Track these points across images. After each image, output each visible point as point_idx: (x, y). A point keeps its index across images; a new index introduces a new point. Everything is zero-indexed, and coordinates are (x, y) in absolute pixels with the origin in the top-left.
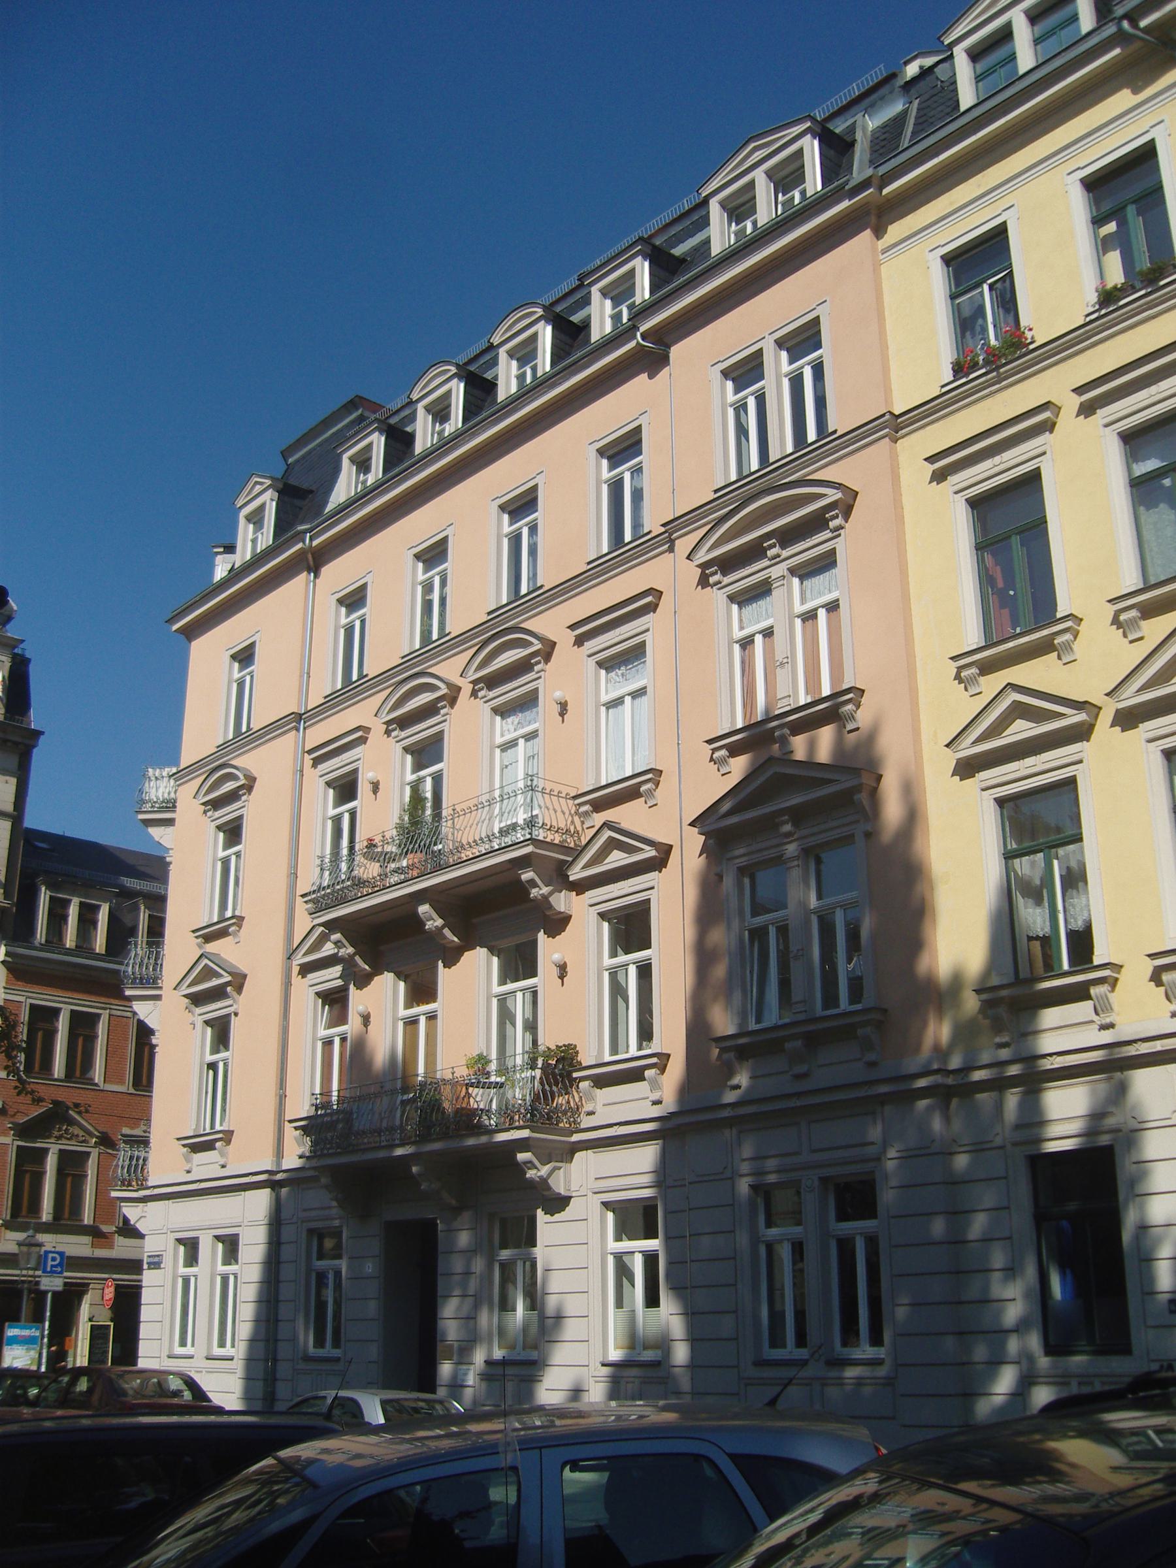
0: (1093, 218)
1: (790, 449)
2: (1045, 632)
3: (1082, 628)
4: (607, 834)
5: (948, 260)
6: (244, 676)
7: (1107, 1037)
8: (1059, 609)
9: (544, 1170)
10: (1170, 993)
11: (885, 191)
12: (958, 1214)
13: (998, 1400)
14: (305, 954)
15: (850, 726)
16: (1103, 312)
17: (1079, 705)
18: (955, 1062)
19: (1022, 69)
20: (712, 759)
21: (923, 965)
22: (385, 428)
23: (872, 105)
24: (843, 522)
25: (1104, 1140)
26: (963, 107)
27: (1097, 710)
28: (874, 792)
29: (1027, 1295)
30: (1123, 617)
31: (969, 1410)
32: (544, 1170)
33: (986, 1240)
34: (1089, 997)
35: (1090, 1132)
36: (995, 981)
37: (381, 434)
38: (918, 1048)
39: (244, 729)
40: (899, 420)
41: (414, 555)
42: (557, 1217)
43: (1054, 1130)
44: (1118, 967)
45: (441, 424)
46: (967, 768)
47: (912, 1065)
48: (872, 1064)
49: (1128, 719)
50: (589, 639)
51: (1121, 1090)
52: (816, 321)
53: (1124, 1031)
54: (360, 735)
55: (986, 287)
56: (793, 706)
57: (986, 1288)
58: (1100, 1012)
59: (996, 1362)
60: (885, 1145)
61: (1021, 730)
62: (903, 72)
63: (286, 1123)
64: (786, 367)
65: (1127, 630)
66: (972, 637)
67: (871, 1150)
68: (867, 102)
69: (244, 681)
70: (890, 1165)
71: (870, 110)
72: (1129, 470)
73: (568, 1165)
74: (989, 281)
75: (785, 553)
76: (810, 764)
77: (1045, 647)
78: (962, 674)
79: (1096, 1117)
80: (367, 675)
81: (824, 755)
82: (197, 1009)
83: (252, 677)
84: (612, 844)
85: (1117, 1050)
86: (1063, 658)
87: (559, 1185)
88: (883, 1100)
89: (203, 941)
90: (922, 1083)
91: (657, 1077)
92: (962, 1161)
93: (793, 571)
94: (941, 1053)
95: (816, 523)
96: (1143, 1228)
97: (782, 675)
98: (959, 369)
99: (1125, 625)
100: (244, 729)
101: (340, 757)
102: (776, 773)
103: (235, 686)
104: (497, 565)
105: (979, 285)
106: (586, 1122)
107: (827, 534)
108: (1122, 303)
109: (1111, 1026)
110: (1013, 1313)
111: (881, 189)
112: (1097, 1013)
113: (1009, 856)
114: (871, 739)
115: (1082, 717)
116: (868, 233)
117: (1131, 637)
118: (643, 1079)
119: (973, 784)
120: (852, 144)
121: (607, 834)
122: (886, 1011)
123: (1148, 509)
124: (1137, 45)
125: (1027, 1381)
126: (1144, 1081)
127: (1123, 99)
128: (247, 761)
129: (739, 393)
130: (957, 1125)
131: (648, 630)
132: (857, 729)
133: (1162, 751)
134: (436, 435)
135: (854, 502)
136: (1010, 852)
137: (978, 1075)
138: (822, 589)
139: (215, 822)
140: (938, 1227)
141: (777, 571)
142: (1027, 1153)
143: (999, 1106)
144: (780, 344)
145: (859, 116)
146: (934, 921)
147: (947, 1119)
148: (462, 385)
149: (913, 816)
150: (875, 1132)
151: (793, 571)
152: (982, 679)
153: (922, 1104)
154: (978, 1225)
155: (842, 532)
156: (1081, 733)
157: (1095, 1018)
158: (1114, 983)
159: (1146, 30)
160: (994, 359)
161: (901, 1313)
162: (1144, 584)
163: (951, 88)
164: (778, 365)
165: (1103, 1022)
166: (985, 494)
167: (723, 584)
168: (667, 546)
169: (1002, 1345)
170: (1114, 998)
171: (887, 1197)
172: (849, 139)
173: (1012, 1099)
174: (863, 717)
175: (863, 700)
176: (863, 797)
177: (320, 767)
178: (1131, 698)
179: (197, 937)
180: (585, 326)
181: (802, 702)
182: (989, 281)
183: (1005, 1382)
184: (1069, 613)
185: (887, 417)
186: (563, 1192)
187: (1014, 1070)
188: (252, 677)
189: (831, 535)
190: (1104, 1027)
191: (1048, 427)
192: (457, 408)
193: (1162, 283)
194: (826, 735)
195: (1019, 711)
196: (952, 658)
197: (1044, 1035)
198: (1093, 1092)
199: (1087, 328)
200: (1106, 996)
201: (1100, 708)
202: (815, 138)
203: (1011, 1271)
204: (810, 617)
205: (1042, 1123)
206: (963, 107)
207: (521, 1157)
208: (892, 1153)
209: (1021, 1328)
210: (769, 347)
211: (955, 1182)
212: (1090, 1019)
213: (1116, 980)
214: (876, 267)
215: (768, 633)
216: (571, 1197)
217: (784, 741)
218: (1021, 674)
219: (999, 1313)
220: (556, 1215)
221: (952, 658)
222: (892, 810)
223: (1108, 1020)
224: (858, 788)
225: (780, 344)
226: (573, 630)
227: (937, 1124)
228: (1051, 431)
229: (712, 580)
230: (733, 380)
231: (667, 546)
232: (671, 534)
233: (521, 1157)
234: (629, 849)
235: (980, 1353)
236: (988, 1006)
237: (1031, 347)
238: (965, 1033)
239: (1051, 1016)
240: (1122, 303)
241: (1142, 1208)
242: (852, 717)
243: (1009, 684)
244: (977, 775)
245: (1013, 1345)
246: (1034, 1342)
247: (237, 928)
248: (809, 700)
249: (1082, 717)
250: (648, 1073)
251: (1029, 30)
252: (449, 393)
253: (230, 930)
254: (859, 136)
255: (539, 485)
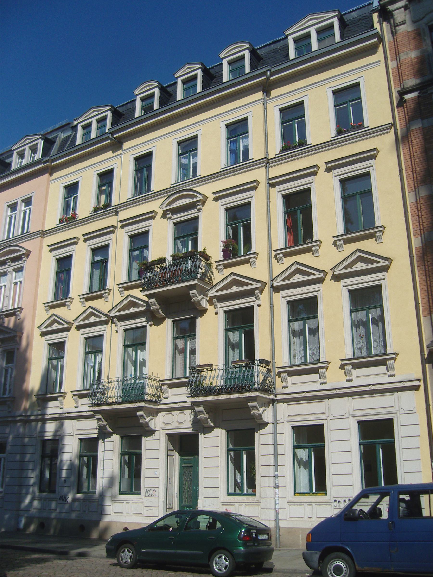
0: (281, 122)
1: (20, 234)
2: (64, 301)
3: (322, 245)
4: (91, 310)
5: (65, 187)
6: (27, 210)
7: (61, 411)
8: (314, 237)
9: (148, 419)
10: (346, 373)
11: (53, 164)
12: (23, 454)
13: (26, 504)
14: (116, 312)
15: (18, 318)
16: (94, 214)
17: (67, 323)
18: (29, 414)
19: (92, 138)
20: (118, 291)
21: (25, 386)
22: (44, 138)
23: (64, 130)
24: (202, 207)
25: (57, 438)
26: (224, 81)
27: (326, 273)
28: (21, 337)
29: (36, 477)
30: (338, 243)
31: (19, 506)
32: (148, 419)
33: (29, 461)
34: (318, 373)
35: (54, 435)
36: (40, 393)
37: (42, 140)
38: (20, 409)
39: (25, 231)
40: (45, 232)
41: (8, 206)
42: (207, 435)
43: (47, 434)
44: (328, 363)
45: (34, 154)
46: (43, 334)
47: (18, 413)
48: (10, 412)
49: (336, 278)
50: (88, 241)
51: (62, 425)
52: (31, 197)
53: (65, 410)
54: (73, 242)
55: (73, 198)
56: (7, 310)
57: (27, 474)
58: (322, 378)
59: (27, 494)
60: (9, 434)
61: (298, 278)
62: (73, 123)
63: (276, 368)
64: (23, 209)
65: (314, 253)
66: (341, 230)
67: (6, 435)
68: (63, 129)
69: (12, 217)
70: (10, 439)
71: (63, 132)
72: (93, 258)
73: (155, 418)
74: (74, 196)
75: (12, 264)
76: (7, 328)
77: (309, 250)
78: (277, 256)
79: (56, 431)
80: (29, 232)
81: (11, 325)
82: (119, 323)
83: (15, 216)
84: (92, 314)
85: (62, 415)
86: (378, 240)
87: (152, 426)
88: (11, 422)
89: (49, 308)
90: (18, 418)
91: (62, 400)
92: (26, 440)
93: (14, 270)
94: (26, 410)
95: (18, 258)
96: (62, 461)
97: (6, 299)
98: (61, 221)
99: (377, 237)
100: (11, 236)
101: (100, 238)
102: (233, 279)
103: (8, 218)
104: (390, 94)
105: (71, 197)
106: (164, 401)
107: (195, 211)
108: (98, 212)
109: (325, 383)
110: (32, 481)
111: (52, 163)
112: (320, 378)
113: (290, 321)
114: (22, 323)
115: (322, 275)
116: (47, 175)
117: (315, 256)
118: (57, 400)
119: (44, 339)
120: (55, 142)
121: (91, 310)
122: (15, 398)
123: (96, 270)
124: (113, 141)
125: (33, 499)
126: (67, 424)
127: (110, 154)
128: (27, 245)
129: (13, 212)
130: (27, 430)
131: (74, 250)
132: (20, 319)
133: (287, 301)
134: (32, 158)
135: (258, 185)
136: (50, 358)
137: (32, 418)
138: (20, 277)
139: (90, 247)
140: (18, 457)
141: (10, 269)
142: (292, 425)
143: (36, 426)
144: (23, 201)
145: (60, 133)
146: (42, 374)
147: (24, 428)
148: (42, 142)
149: (28, 345)
150: (8, 430)
151: (14, 270)
152: (284, 259)
153: (19, 424)
154: (28, 457)
155: (26, 262)
156: (320, 281)
157: (319, 380)
158: (327, 368)
159: (115, 138)
160: (68, 220)
161: (7, 479)
162: (286, 246)
163: (286, 48)
164: (21, 207)
165: (323, 381)
166: (293, 193)
167: (172, 218)
168: (115, 213)
169: (29, 489)
170: (327, 373)
171: (8, 448)
172: (53, 140)
173: (40, 424)
174: (22, 316)
175: (23, 311)
176: (17, 339)
177: (88, 242)
178: (78, 323)
179: (46, 306)
180: (10, 164)
181: (10, 309)
182: (74, 196)
183: (28, 499)
184: (382, 225)
185: (41, 231)
186: (153, 428)
187: (40, 417)
188: (15, 216)
189: (197, 211)
190: (322, 383)
191: (374, 157)
192: (40, 150)
193: (108, 209)
194: (13, 319)
195: (360, 259)
196: (333, 237)
197: (49, 409)
198: (56, 425)
199: (89, 218)
200: (393, 364)
201: (327, 273)
202: (42, 140)
203: (33, 470)
204: (16, 284)
205: (45, 432)
206: (224, 81)
207: (139, 413)
208: (11, 436)
209: (33, 485)
210: (19, 201)
211: (24, 446)
212: (384, 372)
213: (328, 367)
214: (48, 185)
215: (5, 286)
216: (156, 430)
217: (3, 319)
218: (300, 258)
219: (29, 480)
220: (149, 437)
221: (333, 237)
222: (24, 343)
223: (325, 381)
224: (16, 336)
225: (23, 201)
226: (49, 247)
227: (21, 430)
228: (77, 245)
229: (168, 216)
230: (25, 203)
231: (115, 213)
232: (117, 209)
233: (139, 413)
234: (60, 324)
235: (24, 491)
236: (38, 399)
237: (77, 219)
238: (32, 406)
239: (51, 404)
240: (98, 212)
241: (62, 456)
242: (19, 316)
243: (296, 262)
244: (341, 280)
245: (31, 490)
246: (36, 489)
247: (70, 303)
248: (12, 308)
249: (387, 263)
250: (59, 399)
251: (97, 125)
252: (37, 144)
253: (66, 304)
254: (58, 140)
255: (18, 202)
